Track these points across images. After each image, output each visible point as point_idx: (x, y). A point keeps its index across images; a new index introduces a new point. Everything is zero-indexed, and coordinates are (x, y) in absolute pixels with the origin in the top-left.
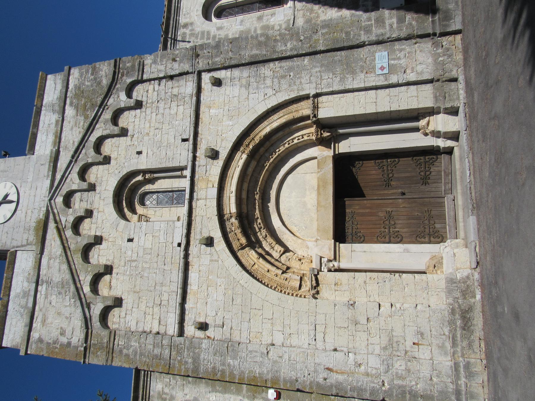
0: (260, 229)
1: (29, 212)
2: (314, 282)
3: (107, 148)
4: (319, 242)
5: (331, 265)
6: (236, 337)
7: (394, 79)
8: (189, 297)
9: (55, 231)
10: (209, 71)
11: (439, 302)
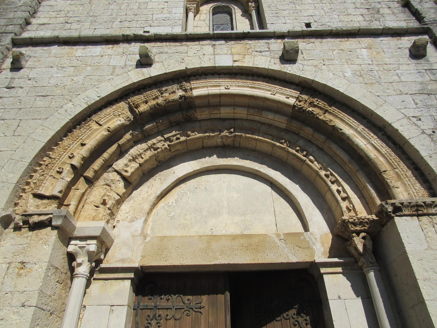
0: (168, 139)
2: (36, 219)
4: (140, 240)
8: (66, 49)
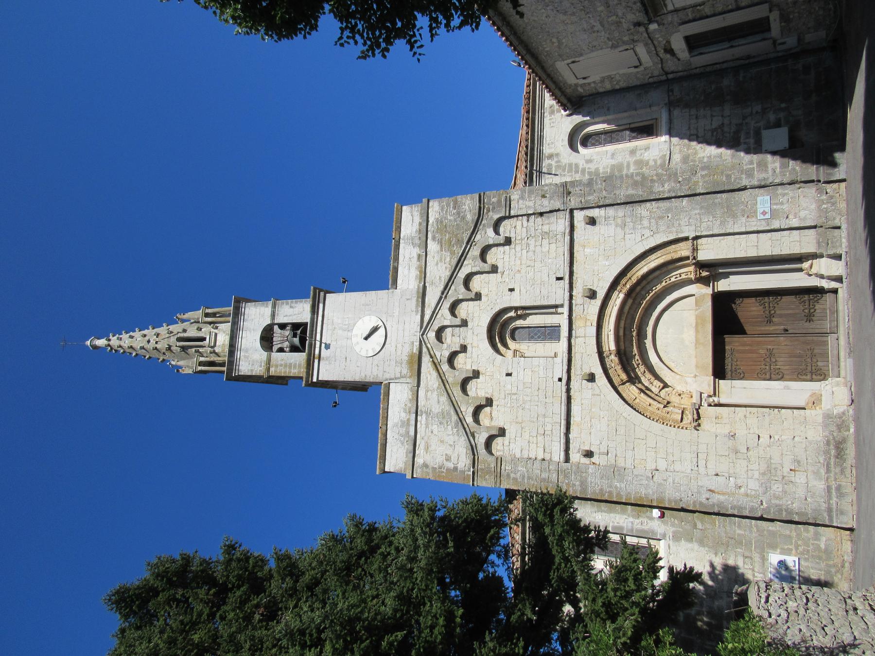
1: (399, 346)
2: (696, 417)
3: (477, 283)
5: (711, 400)
6: (621, 463)
7: (776, 225)
8: (573, 427)
9: (430, 365)
10: (582, 209)
11: (816, 434)
